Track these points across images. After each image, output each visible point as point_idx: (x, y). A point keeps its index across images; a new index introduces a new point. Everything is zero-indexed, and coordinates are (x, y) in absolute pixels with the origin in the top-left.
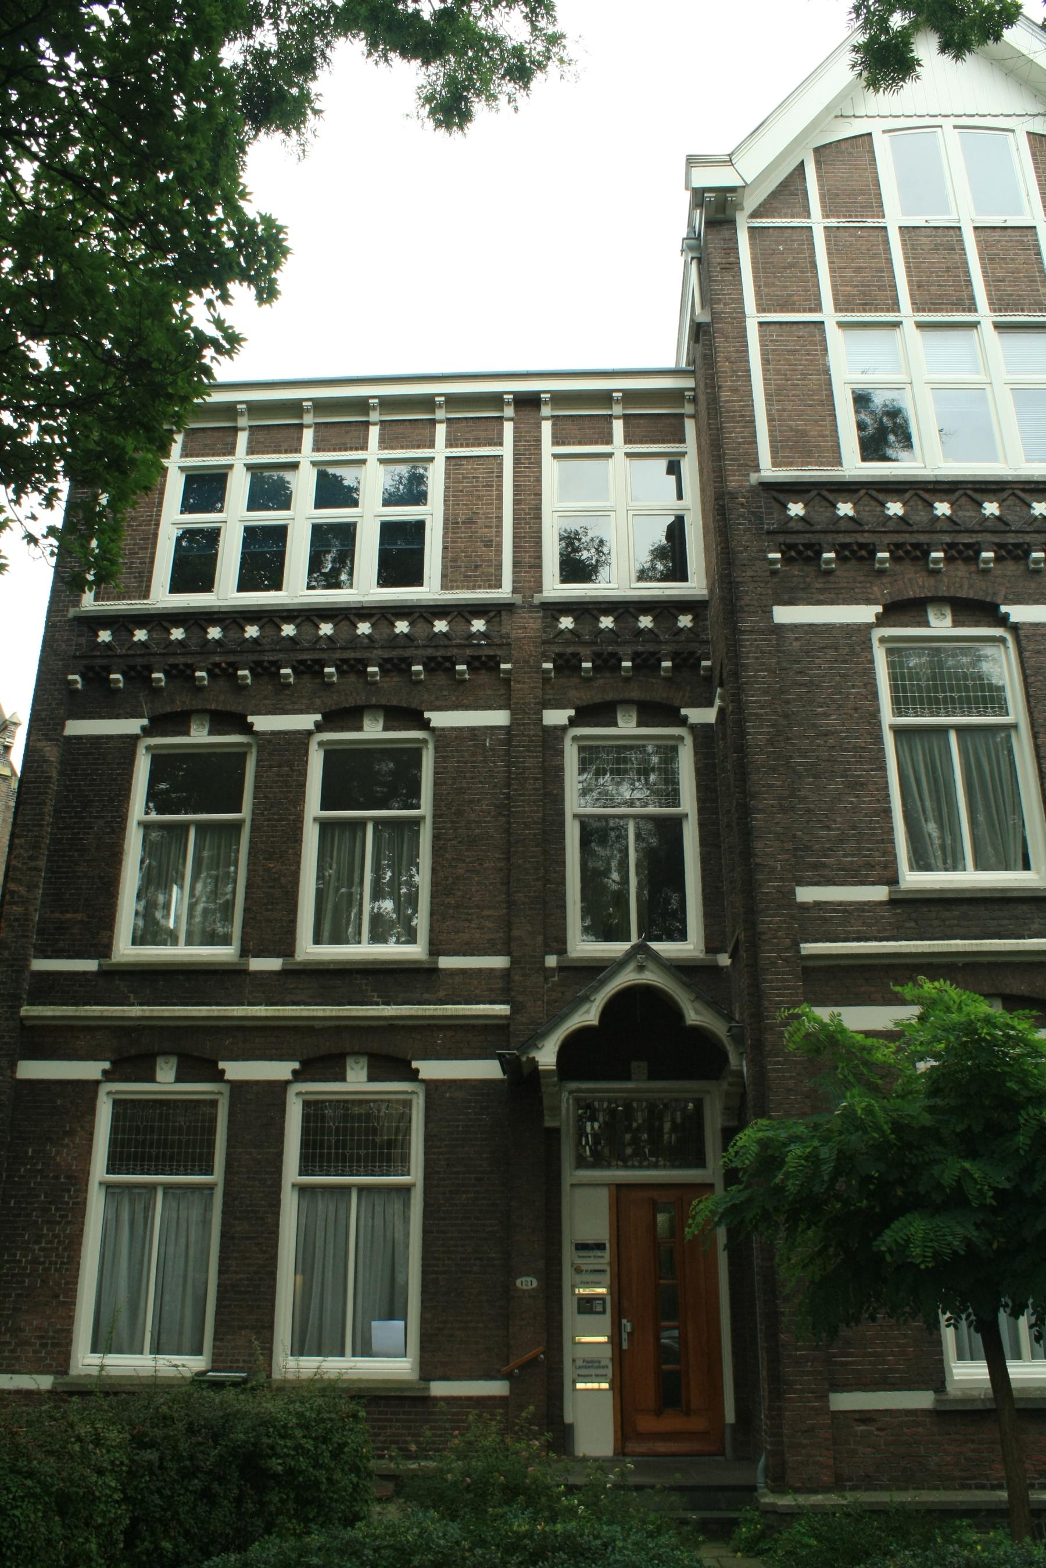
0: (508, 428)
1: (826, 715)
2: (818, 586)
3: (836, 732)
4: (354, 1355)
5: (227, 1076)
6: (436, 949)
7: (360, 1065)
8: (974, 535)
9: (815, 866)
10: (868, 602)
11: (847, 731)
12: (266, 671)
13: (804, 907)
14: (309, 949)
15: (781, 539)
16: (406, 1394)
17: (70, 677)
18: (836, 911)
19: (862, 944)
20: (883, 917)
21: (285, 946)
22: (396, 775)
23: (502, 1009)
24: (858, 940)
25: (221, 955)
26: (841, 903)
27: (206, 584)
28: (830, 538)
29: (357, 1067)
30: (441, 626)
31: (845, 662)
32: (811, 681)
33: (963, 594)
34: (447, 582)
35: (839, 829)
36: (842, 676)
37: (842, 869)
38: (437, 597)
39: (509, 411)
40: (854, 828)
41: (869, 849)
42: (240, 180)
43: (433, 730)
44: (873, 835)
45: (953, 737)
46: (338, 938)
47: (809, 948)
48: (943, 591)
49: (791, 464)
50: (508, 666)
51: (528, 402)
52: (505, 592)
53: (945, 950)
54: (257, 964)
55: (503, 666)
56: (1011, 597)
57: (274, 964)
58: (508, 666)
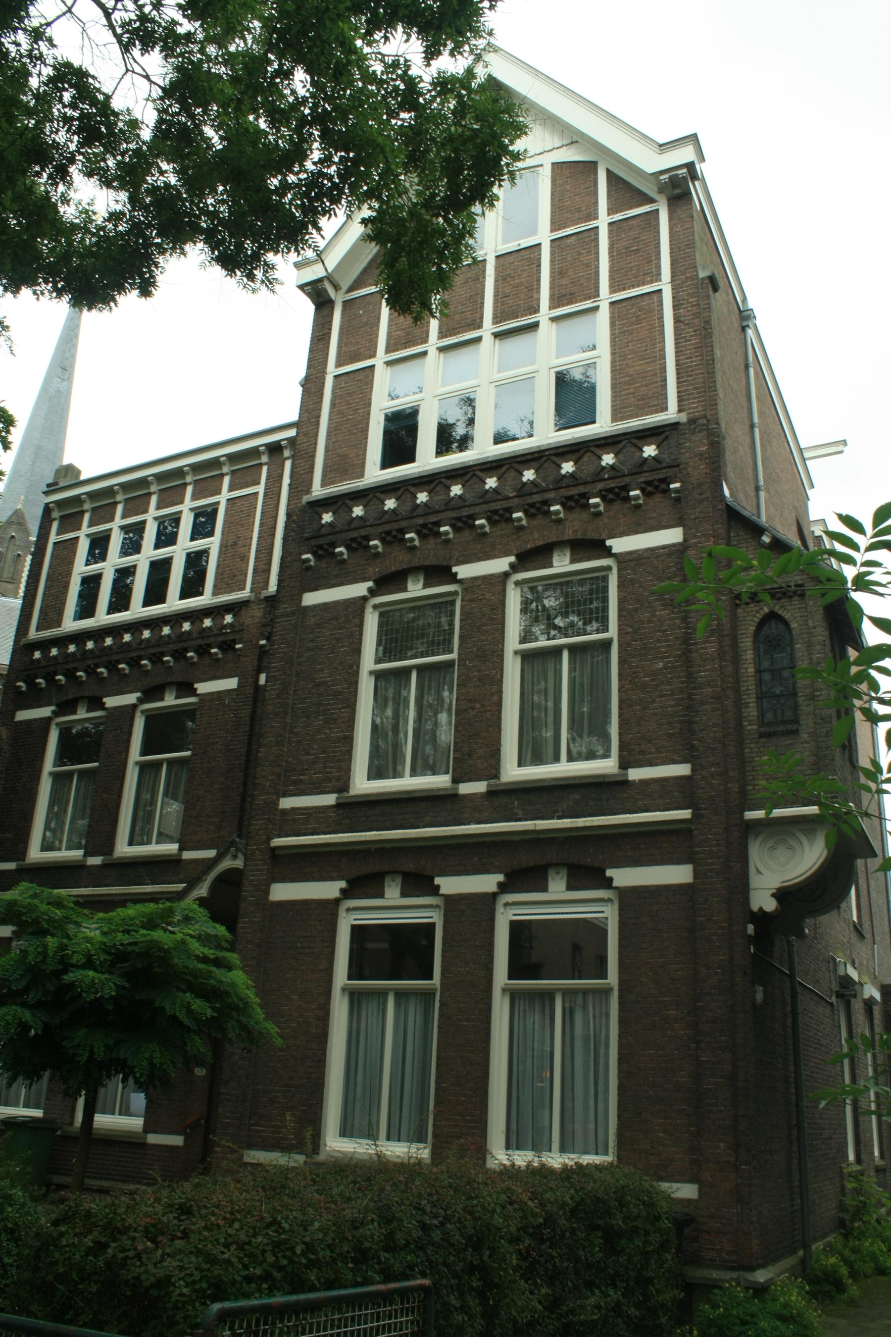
0: (265, 469)
1: (322, 670)
2: (335, 573)
3: (326, 682)
4: (120, 1114)
5: (442, 891)
6: (624, 765)
7: (560, 875)
8: (439, 515)
9: (296, 782)
10: (364, 580)
11: (333, 681)
12: (463, 524)
13: (285, 812)
14: (513, 771)
15: (313, 542)
16: (133, 1140)
17: (304, 557)
18: (303, 814)
19: (315, 837)
20: (330, 817)
21: (493, 771)
22: (584, 600)
23: (685, 814)
24: (312, 834)
25: (441, 782)
26: (306, 808)
27: (410, 457)
28: (343, 536)
29: (557, 877)
30: (207, 623)
31: (341, 628)
32: (317, 646)
33: (428, 563)
34: (216, 592)
35: (314, 754)
36: (337, 639)
37: (311, 784)
38: (608, 429)
39: (265, 459)
40: (324, 752)
41: (331, 768)
42: (85, 310)
43: (615, 556)
44: (335, 756)
45: (565, 655)
46: (538, 759)
47: (277, 842)
48: (416, 562)
49: (333, 483)
50: (677, 485)
51: (275, 449)
52: (671, 413)
53: (363, 839)
54: (466, 788)
55: (672, 486)
56: (461, 559)
57: (479, 787)
58: (677, 485)
